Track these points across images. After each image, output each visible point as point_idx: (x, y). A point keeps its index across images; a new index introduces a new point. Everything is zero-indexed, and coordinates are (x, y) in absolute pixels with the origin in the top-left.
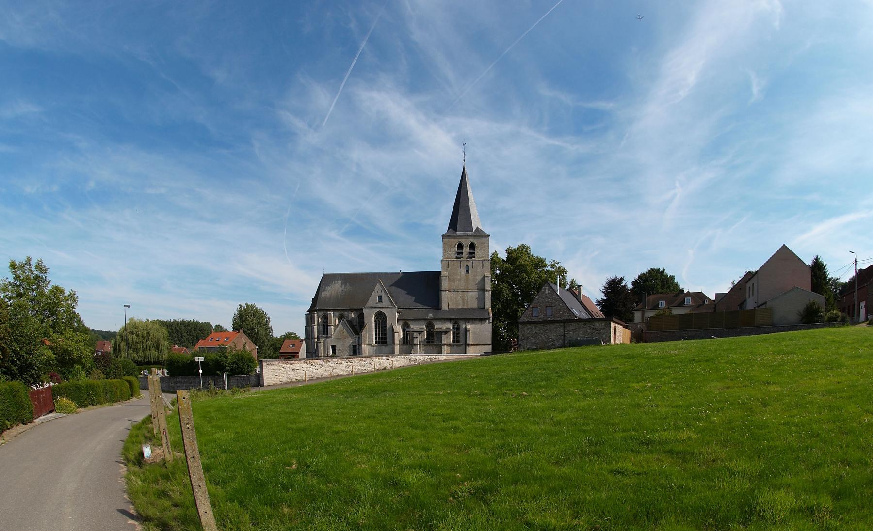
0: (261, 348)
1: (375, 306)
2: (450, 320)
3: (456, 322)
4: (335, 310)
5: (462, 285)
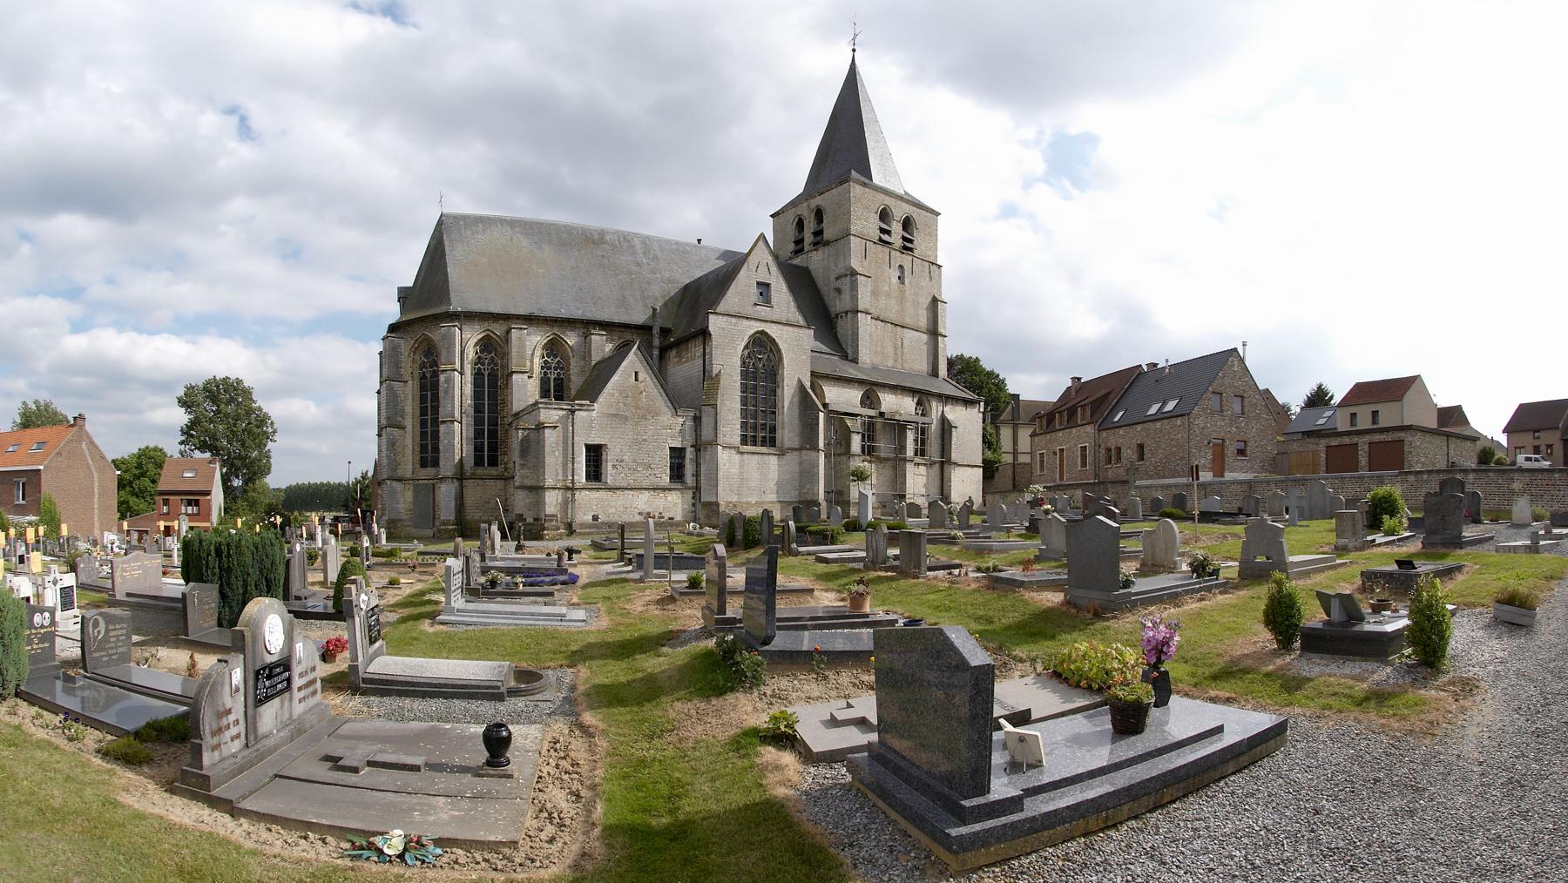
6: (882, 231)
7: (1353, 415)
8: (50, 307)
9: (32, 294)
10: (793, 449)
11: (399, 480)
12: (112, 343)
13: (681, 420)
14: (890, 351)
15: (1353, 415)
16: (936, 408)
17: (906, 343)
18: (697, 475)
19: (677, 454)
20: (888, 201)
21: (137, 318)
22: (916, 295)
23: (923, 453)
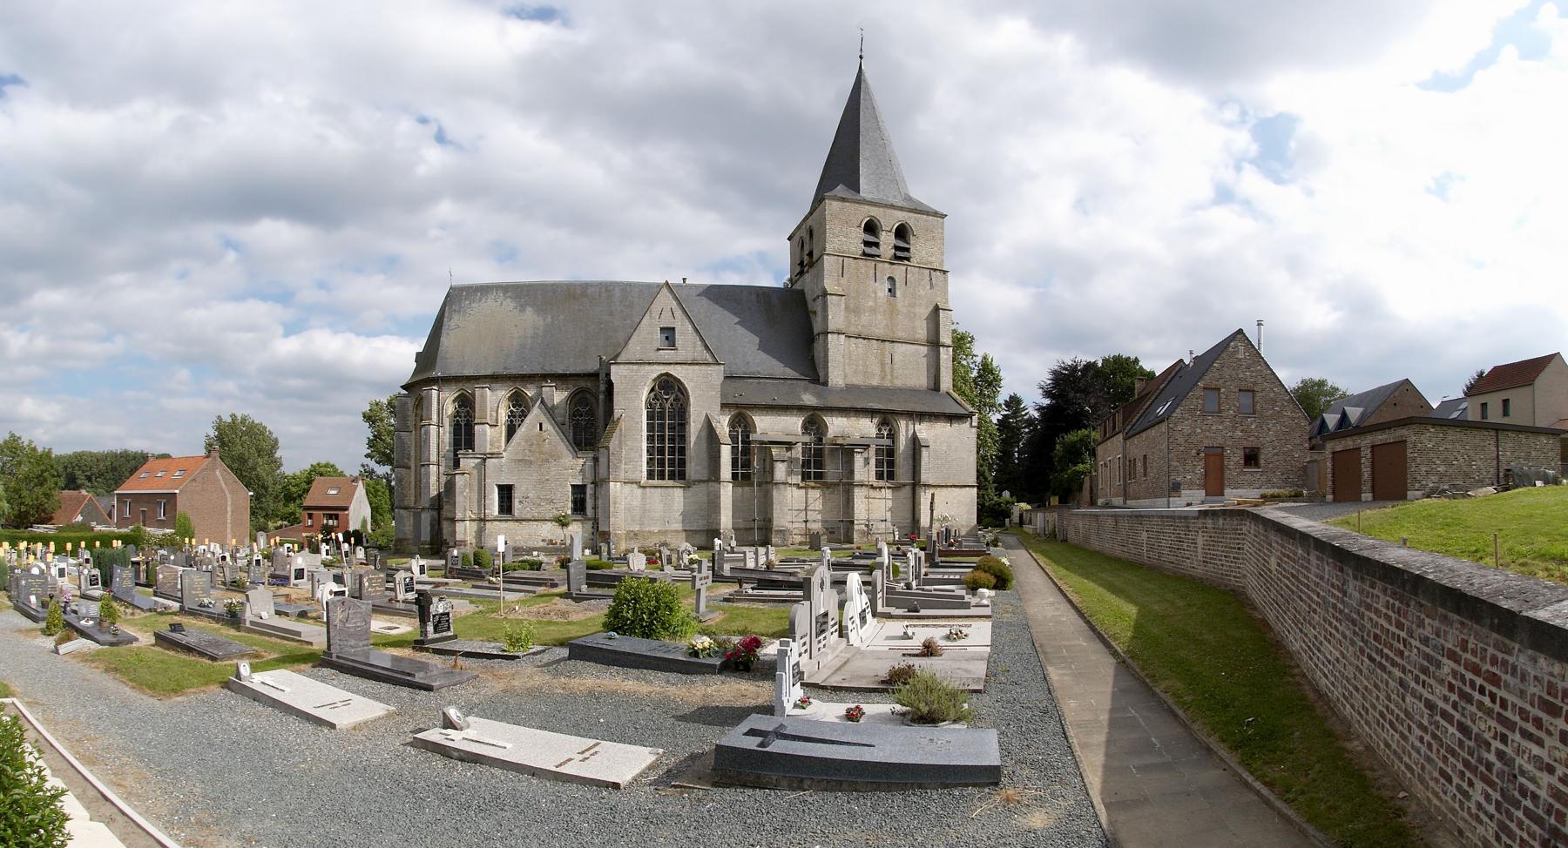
0: (257, 498)
1: (653, 356)
2: (871, 413)
3: (886, 418)
4: (495, 379)
5: (879, 327)
6: (867, 244)
7: (1484, 405)
8: (259, 310)
9: (238, 298)
10: (700, 481)
11: (406, 508)
12: (328, 344)
13: (581, 461)
14: (876, 369)
15: (1484, 405)
16: (904, 429)
17: (896, 358)
18: (595, 508)
19: (578, 490)
20: (875, 212)
21: (345, 318)
22: (912, 305)
23: (891, 476)
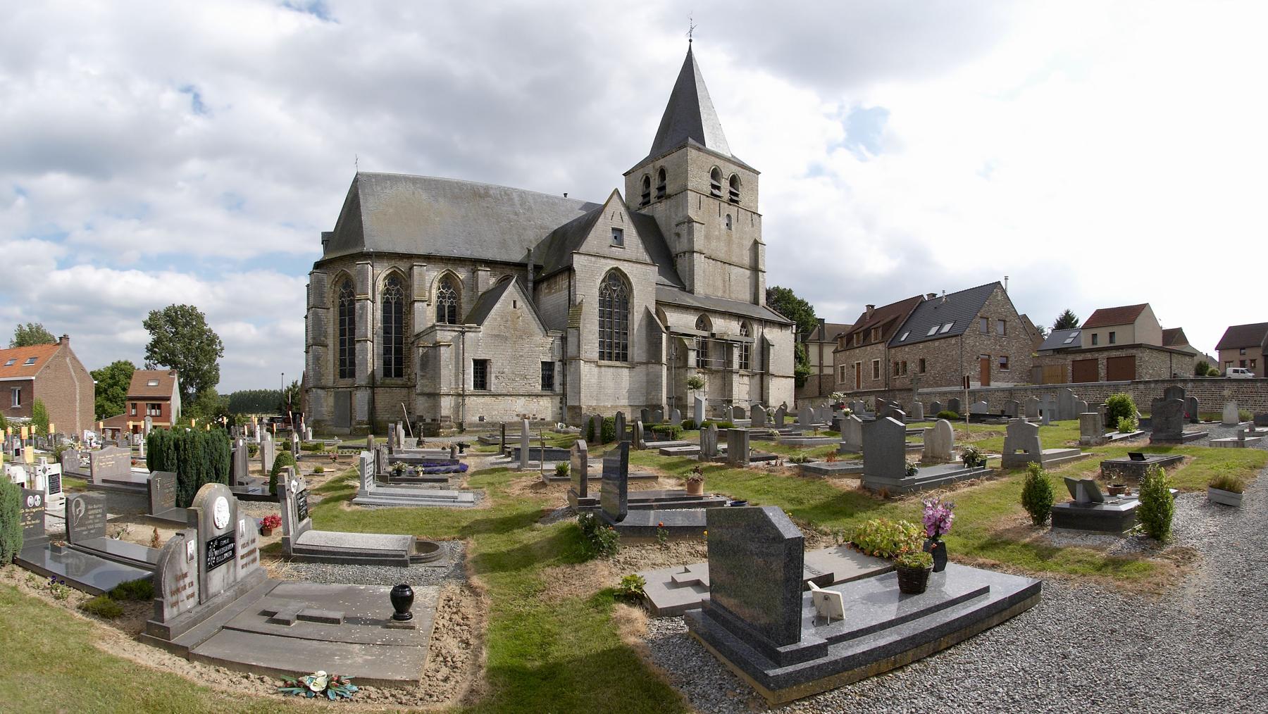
6: (714, 186)
8: (41, 248)
9: (26, 237)
10: (641, 363)
11: (323, 388)
12: (91, 277)
13: (551, 340)
14: (719, 283)
16: (757, 330)
17: (733, 277)
18: (564, 384)
19: (548, 367)
20: (718, 162)
21: (111, 258)
22: (741, 238)
23: (746, 366)
